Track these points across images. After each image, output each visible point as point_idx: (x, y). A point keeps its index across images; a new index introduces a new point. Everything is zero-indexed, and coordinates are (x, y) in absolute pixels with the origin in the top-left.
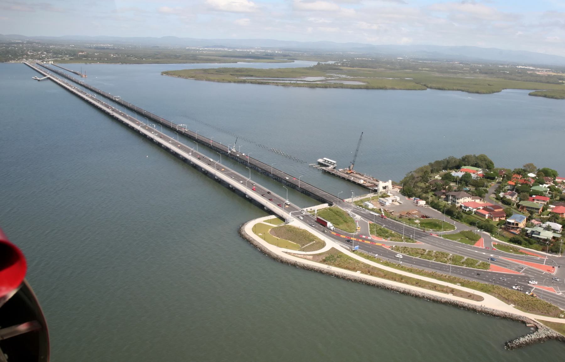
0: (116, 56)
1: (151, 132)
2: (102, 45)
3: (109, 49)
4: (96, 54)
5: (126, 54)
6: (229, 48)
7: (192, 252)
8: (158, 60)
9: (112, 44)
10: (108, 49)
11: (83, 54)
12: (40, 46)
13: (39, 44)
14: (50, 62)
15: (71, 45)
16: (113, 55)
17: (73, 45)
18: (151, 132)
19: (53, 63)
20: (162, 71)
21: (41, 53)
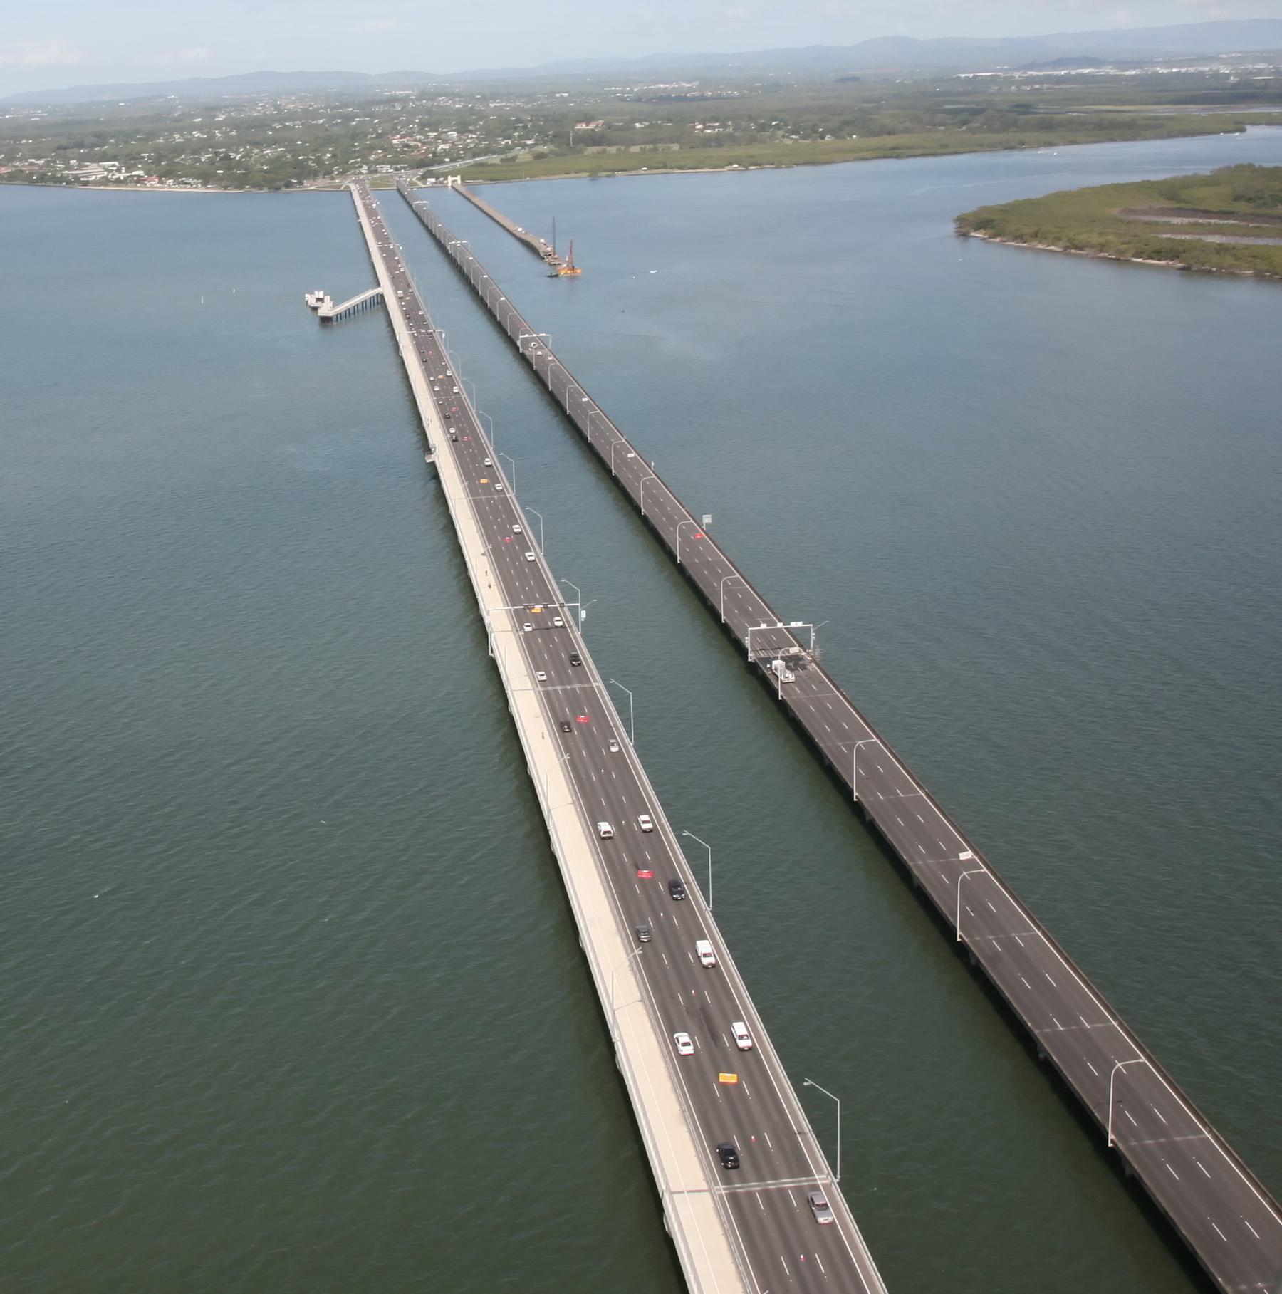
0: (714, 128)
1: (672, 1030)
2: (661, 86)
3: (685, 99)
4: (638, 125)
5: (751, 118)
6: (1118, 64)
7: (314, 832)
8: (889, 141)
9: (696, 80)
10: (681, 99)
11: (591, 127)
12: (457, 106)
13: (457, 99)
14: (450, 179)
15: (558, 95)
16: (704, 124)
17: (566, 95)
18: (672, 1030)
19: (459, 182)
20: (957, 214)
21: (437, 138)
